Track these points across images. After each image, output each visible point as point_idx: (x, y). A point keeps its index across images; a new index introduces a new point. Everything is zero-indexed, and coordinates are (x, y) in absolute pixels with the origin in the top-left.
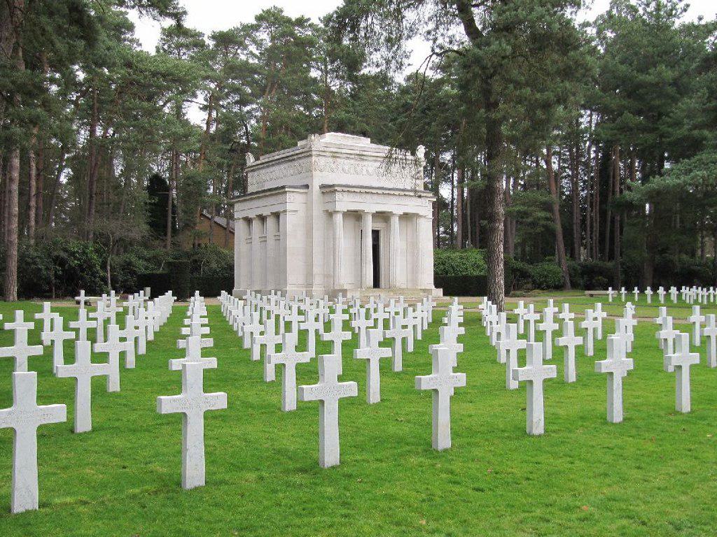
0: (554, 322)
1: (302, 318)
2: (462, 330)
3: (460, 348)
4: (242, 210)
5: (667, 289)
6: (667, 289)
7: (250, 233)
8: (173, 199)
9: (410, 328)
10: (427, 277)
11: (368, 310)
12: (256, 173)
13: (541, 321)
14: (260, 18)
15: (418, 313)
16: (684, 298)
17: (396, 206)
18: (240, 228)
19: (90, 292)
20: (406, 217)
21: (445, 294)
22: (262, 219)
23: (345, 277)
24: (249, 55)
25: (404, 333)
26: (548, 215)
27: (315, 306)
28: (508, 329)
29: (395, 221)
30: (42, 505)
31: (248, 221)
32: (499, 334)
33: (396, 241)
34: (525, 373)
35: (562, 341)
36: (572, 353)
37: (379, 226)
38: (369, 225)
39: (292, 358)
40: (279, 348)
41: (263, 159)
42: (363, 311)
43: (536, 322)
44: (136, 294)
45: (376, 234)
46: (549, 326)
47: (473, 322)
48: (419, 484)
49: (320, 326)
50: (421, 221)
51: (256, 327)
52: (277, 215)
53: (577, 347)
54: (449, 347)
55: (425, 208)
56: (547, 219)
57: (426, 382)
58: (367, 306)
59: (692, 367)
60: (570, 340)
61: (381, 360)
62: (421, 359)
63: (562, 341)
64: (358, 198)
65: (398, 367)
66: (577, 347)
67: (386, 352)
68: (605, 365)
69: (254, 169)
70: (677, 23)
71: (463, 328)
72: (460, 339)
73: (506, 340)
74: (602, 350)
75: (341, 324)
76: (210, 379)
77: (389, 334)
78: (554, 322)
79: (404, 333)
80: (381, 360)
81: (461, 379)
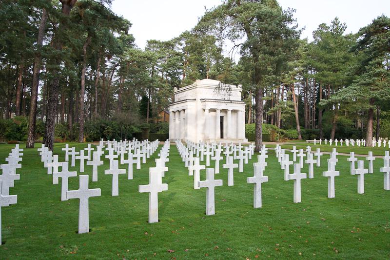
0: (221, 156)
1: (205, 150)
2: (267, 156)
3: (266, 164)
4: (172, 109)
5: (344, 140)
6: (344, 140)
7: (175, 117)
8: (36, 102)
9: (247, 155)
10: (242, 134)
11: (231, 147)
12: (178, 95)
13: (299, 153)
14: (182, 36)
15: (250, 149)
16: (362, 145)
17: (230, 107)
18: (171, 115)
19: (106, 139)
20: (235, 111)
21: (249, 141)
22: (179, 111)
23: (211, 136)
24: (179, 49)
25: (244, 157)
26: (292, 109)
27: (139, 149)
28: (285, 156)
29: (229, 113)
30: (159, 221)
31: (174, 112)
32: (282, 158)
33: (229, 120)
34: (357, 172)
35: (307, 162)
36: (312, 166)
37: (223, 114)
38: (219, 114)
39: (66, 174)
40: (60, 169)
41: (181, 89)
42: (228, 148)
43: (297, 153)
44: (145, 140)
45: (222, 118)
46: (97, 162)
47: (271, 154)
48: (27, 243)
49: (212, 153)
50: (239, 113)
51: (187, 153)
52: (184, 110)
53: (234, 169)
54: (261, 164)
55: (242, 108)
56: (292, 111)
57: (250, 180)
58: (230, 146)
59: (335, 177)
60: (311, 161)
61: (234, 169)
62: (249, 170)
63: (225, 166)
64: (236, 105)
65: (241, 170)
66: (234, 169)
67: (236, 166)
68: (326, 174)
69: (177, 93)
70: (344, 34)
71: (168, 159)
72: (18, 171)
73: (285, 162)
74: (325, 167)
75: (86, 158)
76: (375, 168)
77: (238, 158)
78: (221, 156)
79: (244, 157)
80: (234, 169)
81: (266, 179)
